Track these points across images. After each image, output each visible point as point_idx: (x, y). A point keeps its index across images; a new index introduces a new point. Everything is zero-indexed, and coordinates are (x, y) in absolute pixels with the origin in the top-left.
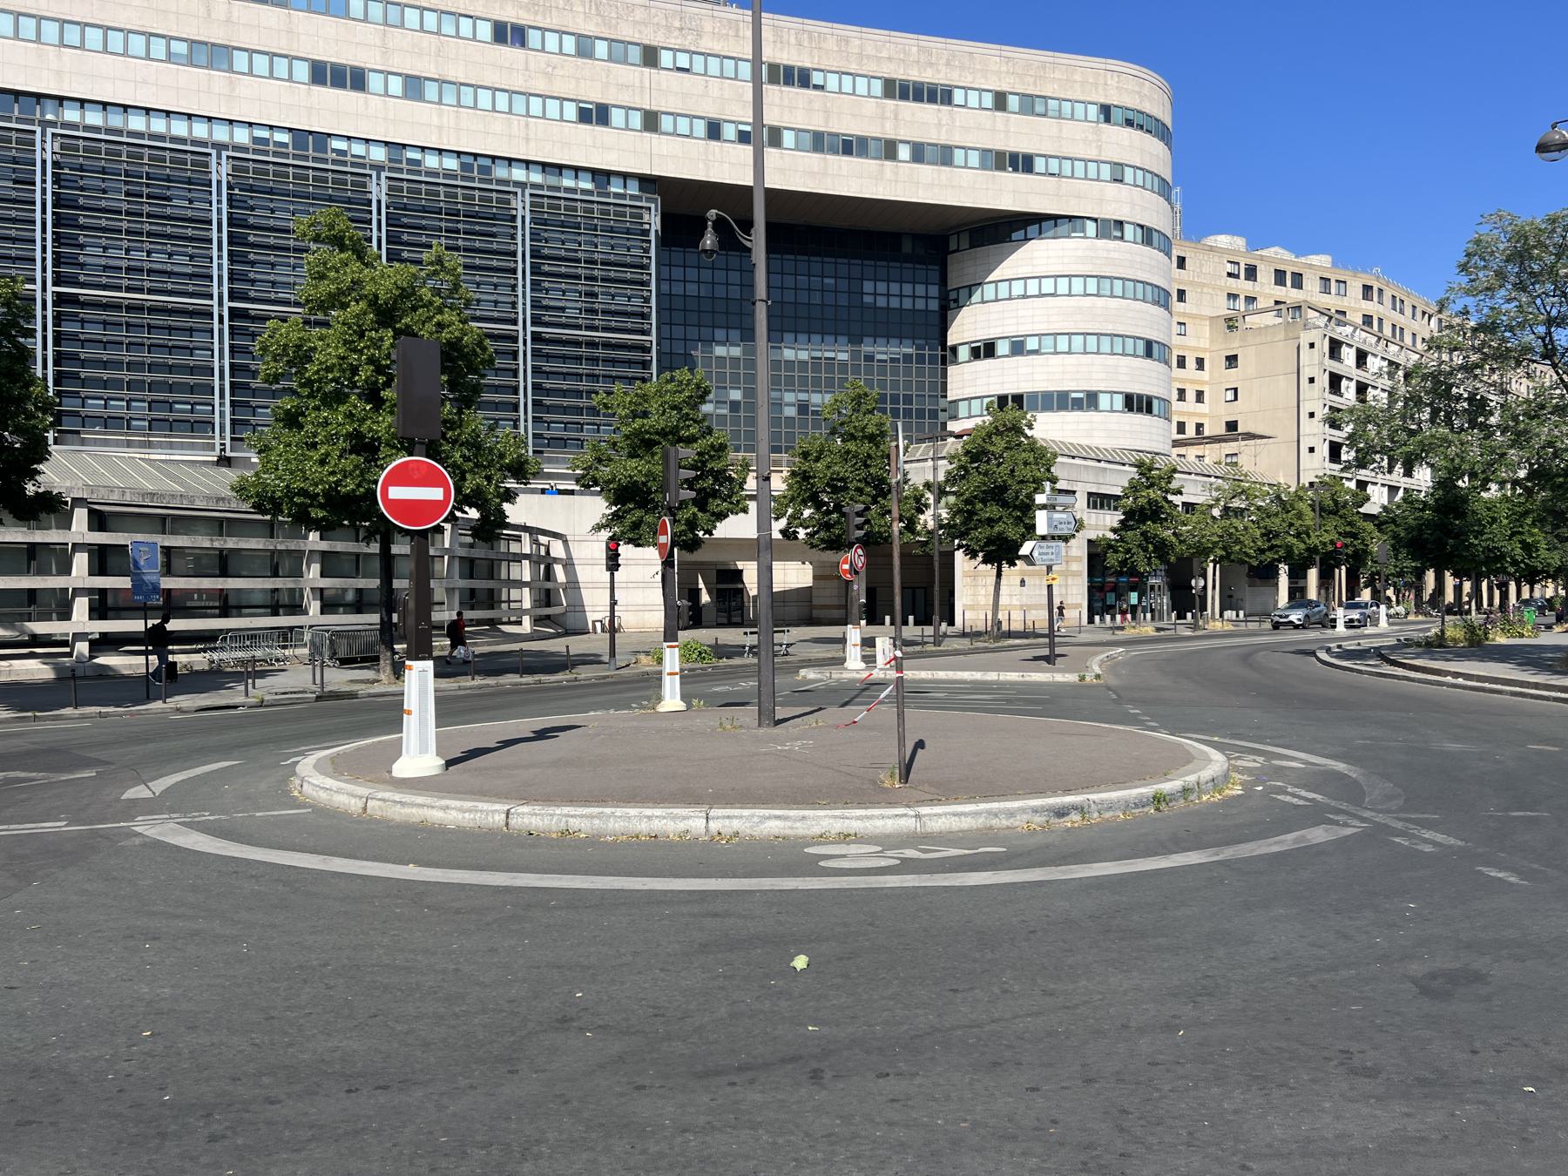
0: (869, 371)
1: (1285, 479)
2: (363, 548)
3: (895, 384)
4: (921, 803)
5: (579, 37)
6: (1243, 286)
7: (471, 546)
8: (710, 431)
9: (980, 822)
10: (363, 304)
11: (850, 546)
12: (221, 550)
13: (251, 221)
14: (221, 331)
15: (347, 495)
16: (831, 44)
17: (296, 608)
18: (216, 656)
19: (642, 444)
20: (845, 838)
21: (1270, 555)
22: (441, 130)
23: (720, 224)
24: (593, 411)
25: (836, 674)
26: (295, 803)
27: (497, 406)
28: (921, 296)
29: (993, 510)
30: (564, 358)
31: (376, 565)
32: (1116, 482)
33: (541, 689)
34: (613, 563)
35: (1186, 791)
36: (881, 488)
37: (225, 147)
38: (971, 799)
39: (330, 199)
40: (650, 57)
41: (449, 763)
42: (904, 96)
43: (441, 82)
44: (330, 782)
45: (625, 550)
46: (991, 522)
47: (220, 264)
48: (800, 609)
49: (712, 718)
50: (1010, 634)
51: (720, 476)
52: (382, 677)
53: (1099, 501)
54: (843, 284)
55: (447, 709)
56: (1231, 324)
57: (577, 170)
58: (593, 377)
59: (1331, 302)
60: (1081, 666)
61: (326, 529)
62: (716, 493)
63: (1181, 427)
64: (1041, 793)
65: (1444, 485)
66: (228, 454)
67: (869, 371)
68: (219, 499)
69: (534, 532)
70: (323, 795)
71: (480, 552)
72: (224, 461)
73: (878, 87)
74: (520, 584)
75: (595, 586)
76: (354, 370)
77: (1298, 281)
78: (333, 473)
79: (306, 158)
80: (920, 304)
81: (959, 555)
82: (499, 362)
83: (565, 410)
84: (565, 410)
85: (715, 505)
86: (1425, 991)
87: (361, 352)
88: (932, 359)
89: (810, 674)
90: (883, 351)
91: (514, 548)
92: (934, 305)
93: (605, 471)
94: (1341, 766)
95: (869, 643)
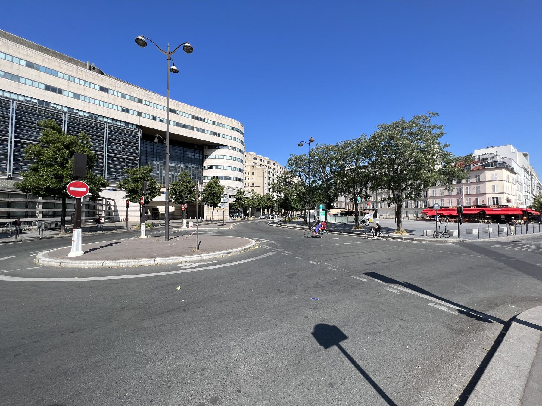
0: (188, 169)
1: (262, 194)
2: (58, 202)
3: (193, 172)
4: (202, 254)
5: (122, 94)
6: (255, 161)
7: (89, 202)
8: (152, 179)
9: (213, 256)
10: (60, 144)
11: (184, 204)
12: (8, 201)
13: (23, 119)
14: (11, 146)
15: (52, 189)
16: (181, 106)
17: (34, 215)
18: (5, 229)
19: (136, 181)
20: (186, 262)
21: (259, 207)
22: (84, 107)
23: (158, 138)
24: (123, 173)
25: (180, 229)
26: (36, 266)
27: (97, 170)
28: (198, 156)
29: (212, 197)
30: (116, 161)
31: (61, 206)
32: (234, 193)
33: (108, 234)
34: (127, 206)
35: (249, 248)
36: (190, 192)
37: (16, 100)
38: (211, 252)
39: (50, 117)
40: (140, 101)
41: (85, 253)
42: (195, 119)
43: (85, 96)
44: (48, 259)
45: (131, 203)
46: (212, 199)
47: (12, 129)
48: (173, 216)
49: (154, 239)
50: (215, 221)
51: (155, 188)
52: (61, 233)
53: (231, 196)
54: (182, 152)
55: (85, 240)
56: (253, 167)
57: (121, 121)
58: (124, 166)
59: (268, 165)
60: (229, 226)
61: (44, 197)
62: (155, 192)
63: (245, 184)
64: (224, 250)
65: (286, 196)
66: (11, 176)
67: (188, 169)
68: (8, 188)
69: (106, 199)
70: (46, 263)
71: (91, 203)
72: (9, 178)
73: (190, 116)
74: (102, 211)
75: (122, 211)
76: (57, 159)
77: (264, 161)
78: (48, 183)
79: (43, 107)
80: (198, 158)
81: (206, 206)
82: (99, 160)
83: (116, 172)
84: (116, 172)
85: (153, 194)
86: (289, 278)
87: (59, 155)
88: (200, 168)
89: (175, 229)
90: (191, 166)
91: (101, 202)
92: (201, 158)
93: (126, 186)
94: (273, 242)
95: (188, 223)
